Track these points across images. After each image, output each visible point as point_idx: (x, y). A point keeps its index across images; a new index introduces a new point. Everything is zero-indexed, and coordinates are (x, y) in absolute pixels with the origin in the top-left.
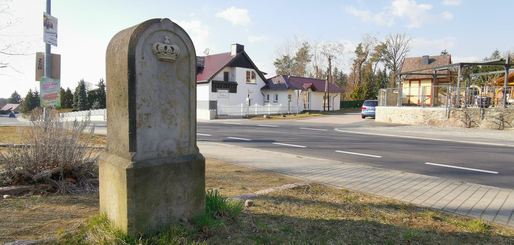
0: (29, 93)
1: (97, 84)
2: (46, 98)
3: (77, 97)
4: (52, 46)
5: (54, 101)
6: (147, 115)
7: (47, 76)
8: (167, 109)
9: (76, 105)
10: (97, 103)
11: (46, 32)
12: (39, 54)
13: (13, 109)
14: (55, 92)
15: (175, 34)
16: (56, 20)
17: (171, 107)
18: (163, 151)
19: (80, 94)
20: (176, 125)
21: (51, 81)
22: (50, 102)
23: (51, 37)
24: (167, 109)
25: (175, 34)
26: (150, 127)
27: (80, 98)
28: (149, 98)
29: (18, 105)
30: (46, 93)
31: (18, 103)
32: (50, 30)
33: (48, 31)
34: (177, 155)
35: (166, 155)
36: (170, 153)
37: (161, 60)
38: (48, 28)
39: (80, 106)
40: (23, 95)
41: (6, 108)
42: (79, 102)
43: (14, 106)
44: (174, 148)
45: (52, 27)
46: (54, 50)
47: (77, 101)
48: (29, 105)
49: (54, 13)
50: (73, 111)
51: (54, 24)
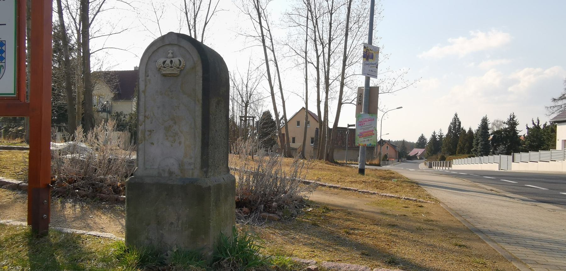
0: (433, 136)
1: (506, 121)
2: (361, 135)
3: (478, 140)
4: (371, 78)
5: (369, 139)
6: (150, 131)
7: (365, 112)
8: (170, 126)
9: (476, 150)
10: (501, 147)
11: (364, 64)
12: (360, 89)
13: (418, 155)
14: (371, 129)
15: (180, 46)
16: (377, 50)
17: (175, 123)
18: (164, 171)
19: (482, 135)
20: (180, 143)
21: (368, 116)
22: (366, 140)
23: (371, 69)
24: (170, 126)
25: (180, 46)
26: (153, 144)
27: (481, 141)
28: (152, 115)
29: (423, 150)
30: (362, 131)
31: (424, 148)
32: (370, 61)
33: (367, 63)
34: (179, 177)
35: (166, 175)
36: (171, 173)
37: (164, 75)
38: (367, 59)
39: (480, 152)
40: (428, 138)
41: (412, 153)
42: (480, 145)
43: (420, 151)
44: (175, 169)
45: (372, 58)
46: (373, 82)
47: (477, 144)
48: (432, 150)
49: (375, 43)
50: (470, 157)
51: (374, 54)
